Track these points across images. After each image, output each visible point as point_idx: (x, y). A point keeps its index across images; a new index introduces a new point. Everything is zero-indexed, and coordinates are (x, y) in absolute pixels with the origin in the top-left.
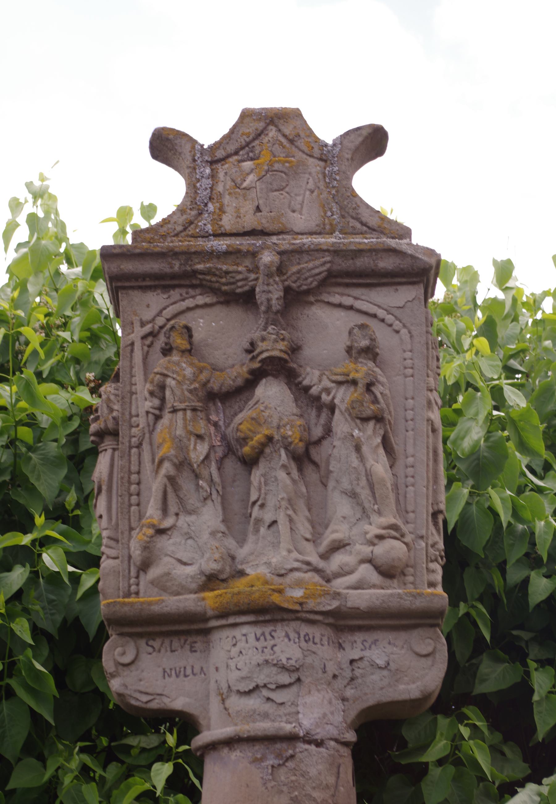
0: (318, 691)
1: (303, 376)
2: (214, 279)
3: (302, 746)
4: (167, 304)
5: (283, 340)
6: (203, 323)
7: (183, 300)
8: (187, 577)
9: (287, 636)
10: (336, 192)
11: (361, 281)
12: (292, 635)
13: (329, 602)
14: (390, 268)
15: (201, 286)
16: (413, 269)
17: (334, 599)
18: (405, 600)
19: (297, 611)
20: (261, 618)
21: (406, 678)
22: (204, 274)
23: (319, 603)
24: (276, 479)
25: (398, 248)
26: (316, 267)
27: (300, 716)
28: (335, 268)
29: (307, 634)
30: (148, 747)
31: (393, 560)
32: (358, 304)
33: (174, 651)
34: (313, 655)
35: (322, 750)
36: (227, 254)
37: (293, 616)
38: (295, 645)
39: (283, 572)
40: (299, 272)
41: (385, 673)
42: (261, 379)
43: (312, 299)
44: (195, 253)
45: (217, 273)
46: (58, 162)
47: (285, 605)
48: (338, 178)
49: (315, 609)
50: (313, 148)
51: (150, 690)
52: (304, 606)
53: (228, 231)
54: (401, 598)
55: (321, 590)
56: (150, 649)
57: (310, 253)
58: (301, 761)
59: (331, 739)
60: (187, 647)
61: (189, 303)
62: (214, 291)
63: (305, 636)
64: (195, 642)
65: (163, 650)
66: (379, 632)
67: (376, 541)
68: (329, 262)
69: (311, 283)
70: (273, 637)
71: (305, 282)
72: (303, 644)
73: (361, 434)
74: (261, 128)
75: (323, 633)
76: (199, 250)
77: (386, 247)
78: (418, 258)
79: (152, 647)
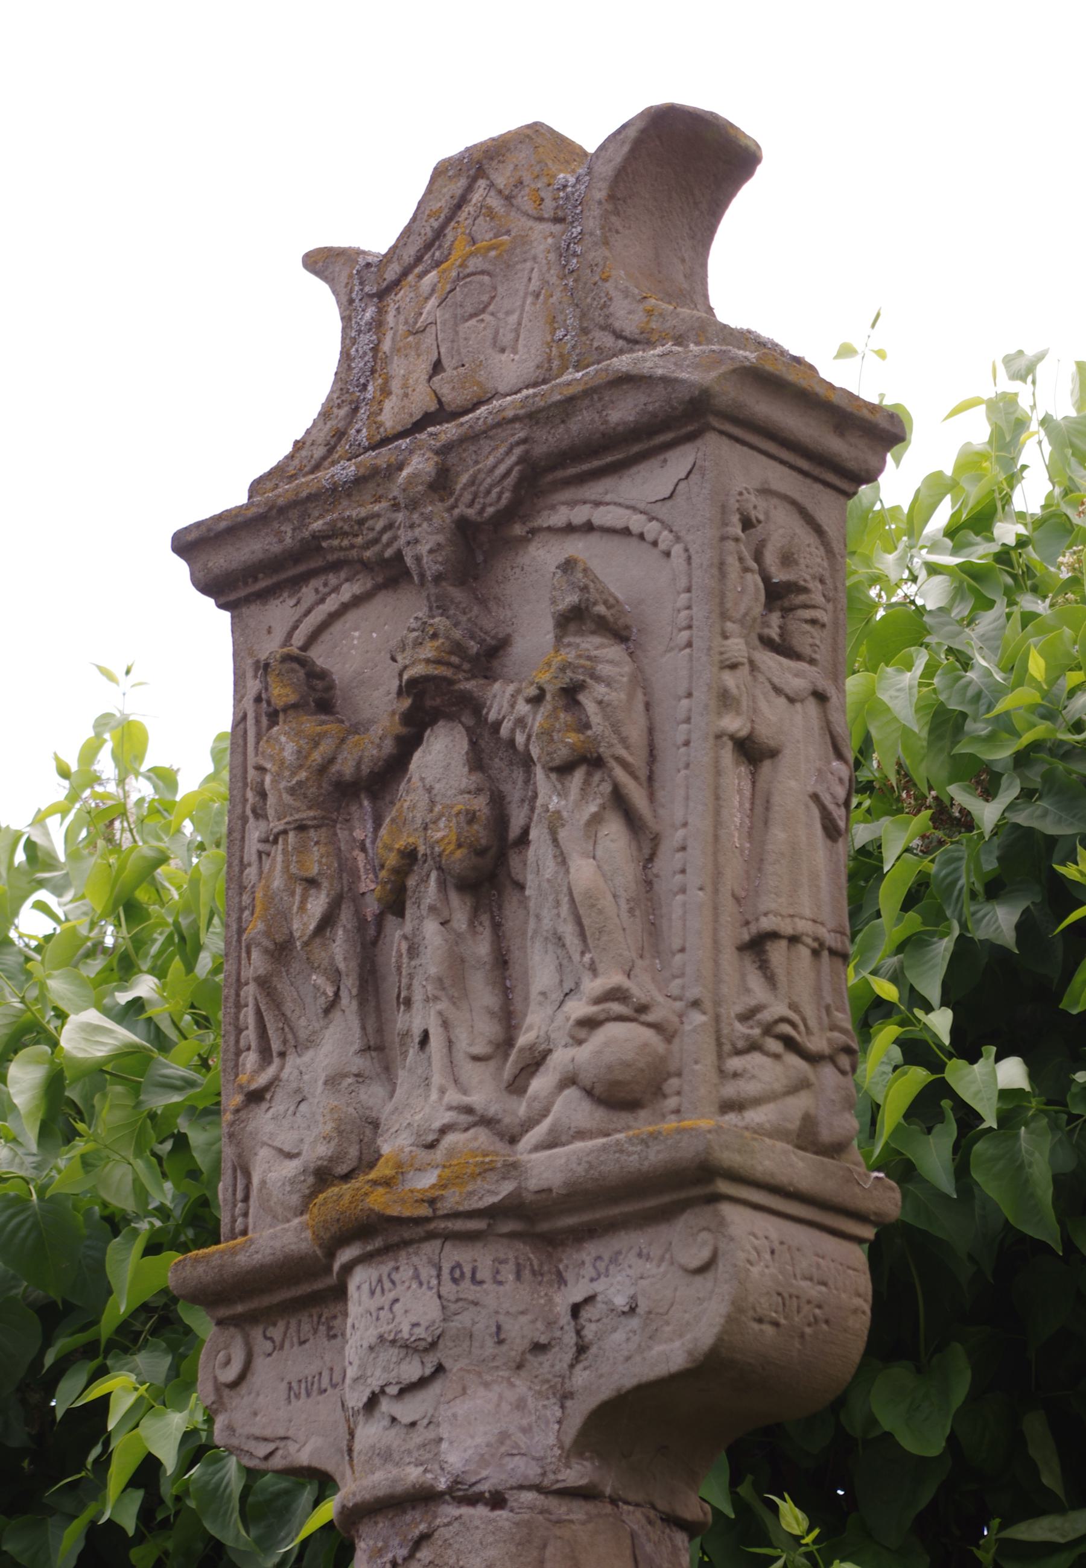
0: (486, 1385)
1: (488, 703)
2: (345, 543)
3: (451, 1511)
4: (296, 617)
5: (435, 636)
6: (360, 637)
7: (322, 601)
8: (284, 1184)
9: (417, 1276)
10: (575, 281)
11: (596, 463)
12: (427, 1272)
13: (493, 1187)
14: (631, 418)
15: (335, 567)
16: (674, 408)
17: (504, 1178)
18: (629, 1154)
19: (427, 1220)
20: (369, 1248)
21: (667, 1329)
22: (329, 537)
23: (471, 1193)
24: (431, 935)
25: (635, 372)
26: (500, 461)
27: (444, 1445)
28: (539, 450)
29: (458, 1265)
30: (1062, 1541)
31: (610, 1068)
32: (604, 516)
33: (304, 1342)
34: (472, 1308)
35: (503, 1514)
36: (359, 481)
37: (420, 1231)
38: (430, 1293)
39: (431, 1137)
40: (472, 482)
41: (634, 1323)
42: (425, 730)
43: (518, 530)
44: (310, 498)
45: (346, 528)
46: (878, 315)
47: (395, 1211)
48: (578, 249)
49: (461, 1208)
50: (542, 200)
51: (268, 1433)
52: (439, 1205)
53: (390, 432)
54: (621, 1151)
55: (476, 1165)
56: (268, 1346)
57: (491, 433)
58: (447, 1544)
59: (521, 1487)
60: (322, 1329)
61: (332, 604)
62: (366, 566)
63: (453, 1269)
64: (335, 1317)
65: (287, 1345)
66: (623, 1233)
67: (582, 1033)
68: (524, 441)
69: (499, 498)
70: (393, 1282)
71: (488, 500)
72: (448, 1288)
73: (563, 803)
74: (459, 192)
75: (502, 1256)
76: (314, 490)
77: (611, 378)
78: (676, 380)
79: (271, 1339)
